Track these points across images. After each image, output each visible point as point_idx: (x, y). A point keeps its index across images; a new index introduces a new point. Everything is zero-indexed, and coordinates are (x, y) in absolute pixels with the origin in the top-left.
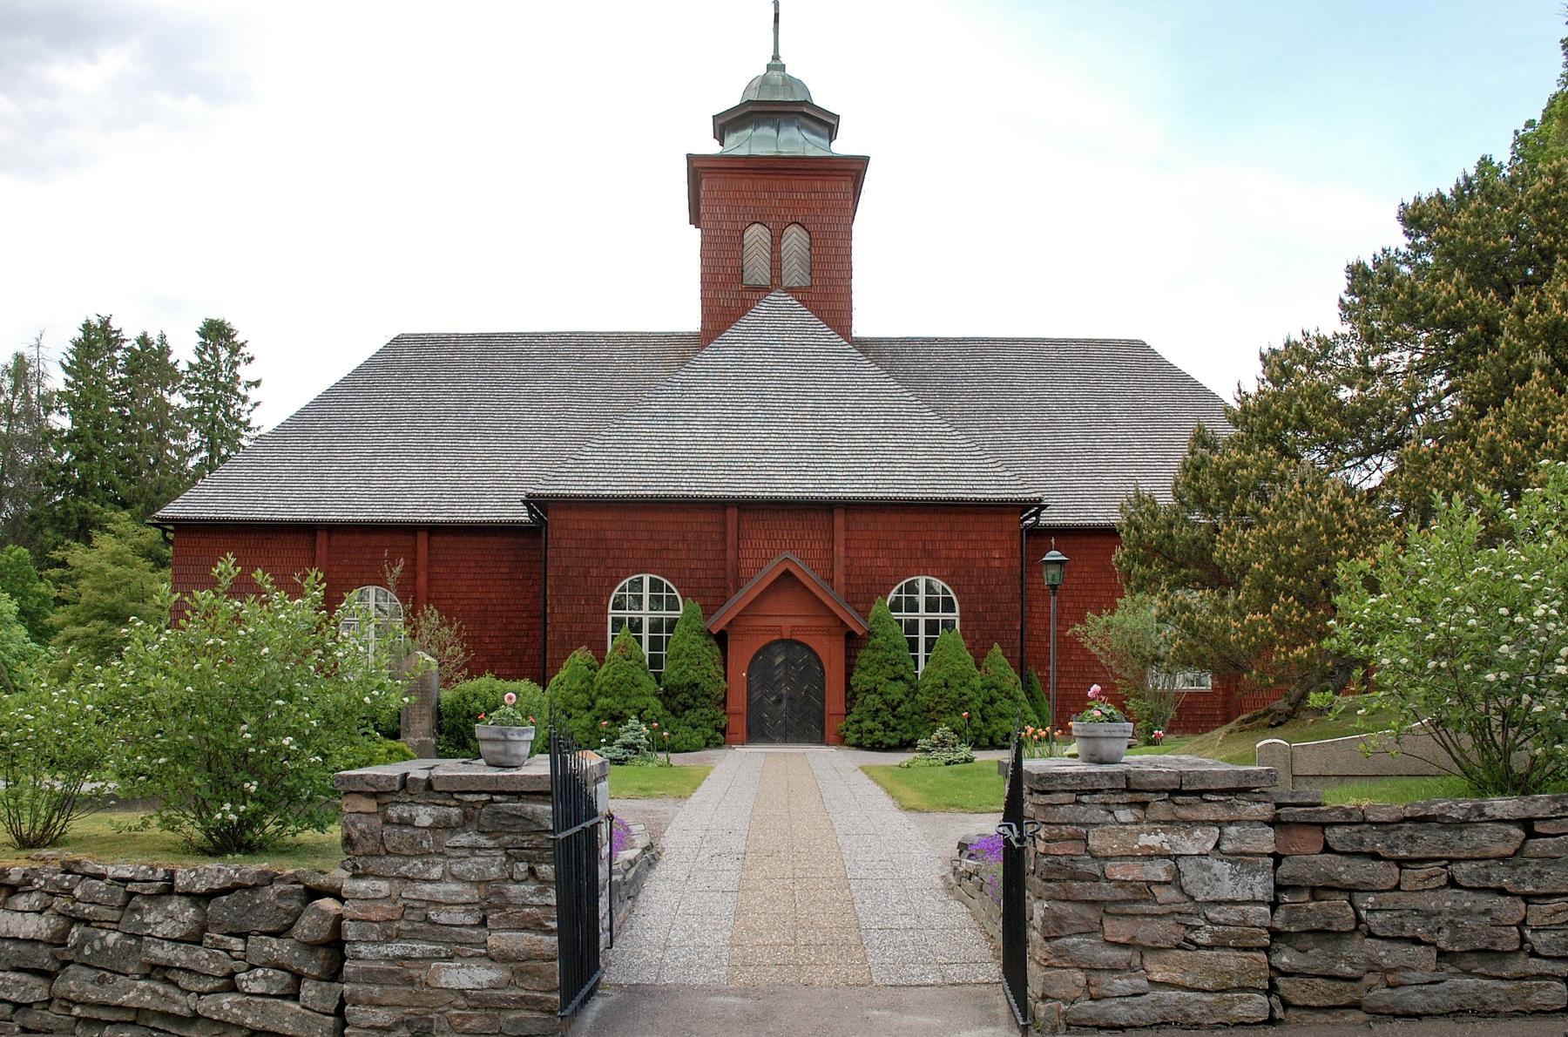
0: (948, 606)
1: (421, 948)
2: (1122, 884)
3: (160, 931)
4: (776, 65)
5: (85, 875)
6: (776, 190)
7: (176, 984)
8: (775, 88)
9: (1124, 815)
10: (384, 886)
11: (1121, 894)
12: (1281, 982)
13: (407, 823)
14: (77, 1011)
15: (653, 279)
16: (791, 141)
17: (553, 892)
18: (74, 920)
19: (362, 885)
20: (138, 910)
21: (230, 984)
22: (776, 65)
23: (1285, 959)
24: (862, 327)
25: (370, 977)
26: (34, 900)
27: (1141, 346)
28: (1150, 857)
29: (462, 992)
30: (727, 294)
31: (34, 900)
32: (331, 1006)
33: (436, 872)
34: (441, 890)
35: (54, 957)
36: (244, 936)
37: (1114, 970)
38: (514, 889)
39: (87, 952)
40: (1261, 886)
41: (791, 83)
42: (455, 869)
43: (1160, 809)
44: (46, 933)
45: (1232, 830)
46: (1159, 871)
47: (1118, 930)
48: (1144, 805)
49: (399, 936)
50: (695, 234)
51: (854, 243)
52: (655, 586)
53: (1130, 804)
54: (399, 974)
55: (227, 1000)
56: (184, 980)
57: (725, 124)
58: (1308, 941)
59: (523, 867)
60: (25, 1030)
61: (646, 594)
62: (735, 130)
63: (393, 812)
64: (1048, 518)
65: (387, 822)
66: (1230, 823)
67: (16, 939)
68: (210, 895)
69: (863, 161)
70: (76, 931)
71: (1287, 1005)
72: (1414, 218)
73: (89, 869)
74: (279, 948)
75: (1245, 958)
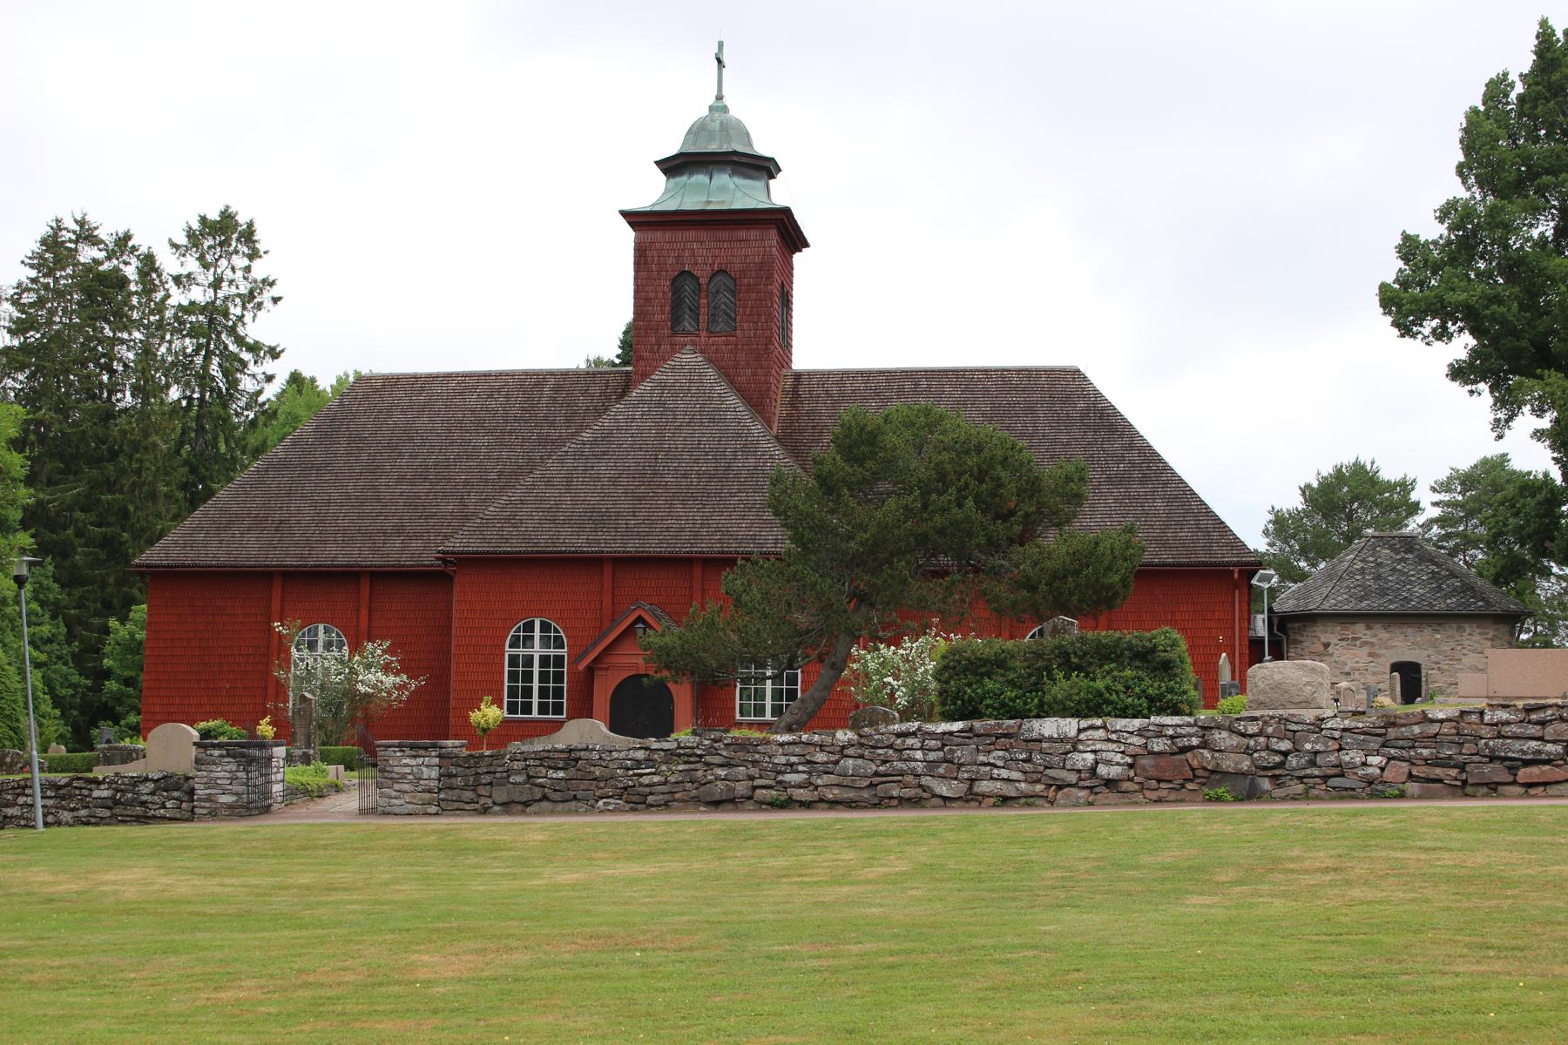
4: (719, 106)
16: (723, 189)
18: (117, 791)
22: (719, 106)
25: (200, 800)
27: (1076, 373)
34: (221, 774)
40: (434, 773)
43: (408, 752)
46: (408, 770)
47: (396, 786)
51: (795, 279)
52: (545, 627)
54: (209, 799)
57: (672, 166)
74: (176, 794)
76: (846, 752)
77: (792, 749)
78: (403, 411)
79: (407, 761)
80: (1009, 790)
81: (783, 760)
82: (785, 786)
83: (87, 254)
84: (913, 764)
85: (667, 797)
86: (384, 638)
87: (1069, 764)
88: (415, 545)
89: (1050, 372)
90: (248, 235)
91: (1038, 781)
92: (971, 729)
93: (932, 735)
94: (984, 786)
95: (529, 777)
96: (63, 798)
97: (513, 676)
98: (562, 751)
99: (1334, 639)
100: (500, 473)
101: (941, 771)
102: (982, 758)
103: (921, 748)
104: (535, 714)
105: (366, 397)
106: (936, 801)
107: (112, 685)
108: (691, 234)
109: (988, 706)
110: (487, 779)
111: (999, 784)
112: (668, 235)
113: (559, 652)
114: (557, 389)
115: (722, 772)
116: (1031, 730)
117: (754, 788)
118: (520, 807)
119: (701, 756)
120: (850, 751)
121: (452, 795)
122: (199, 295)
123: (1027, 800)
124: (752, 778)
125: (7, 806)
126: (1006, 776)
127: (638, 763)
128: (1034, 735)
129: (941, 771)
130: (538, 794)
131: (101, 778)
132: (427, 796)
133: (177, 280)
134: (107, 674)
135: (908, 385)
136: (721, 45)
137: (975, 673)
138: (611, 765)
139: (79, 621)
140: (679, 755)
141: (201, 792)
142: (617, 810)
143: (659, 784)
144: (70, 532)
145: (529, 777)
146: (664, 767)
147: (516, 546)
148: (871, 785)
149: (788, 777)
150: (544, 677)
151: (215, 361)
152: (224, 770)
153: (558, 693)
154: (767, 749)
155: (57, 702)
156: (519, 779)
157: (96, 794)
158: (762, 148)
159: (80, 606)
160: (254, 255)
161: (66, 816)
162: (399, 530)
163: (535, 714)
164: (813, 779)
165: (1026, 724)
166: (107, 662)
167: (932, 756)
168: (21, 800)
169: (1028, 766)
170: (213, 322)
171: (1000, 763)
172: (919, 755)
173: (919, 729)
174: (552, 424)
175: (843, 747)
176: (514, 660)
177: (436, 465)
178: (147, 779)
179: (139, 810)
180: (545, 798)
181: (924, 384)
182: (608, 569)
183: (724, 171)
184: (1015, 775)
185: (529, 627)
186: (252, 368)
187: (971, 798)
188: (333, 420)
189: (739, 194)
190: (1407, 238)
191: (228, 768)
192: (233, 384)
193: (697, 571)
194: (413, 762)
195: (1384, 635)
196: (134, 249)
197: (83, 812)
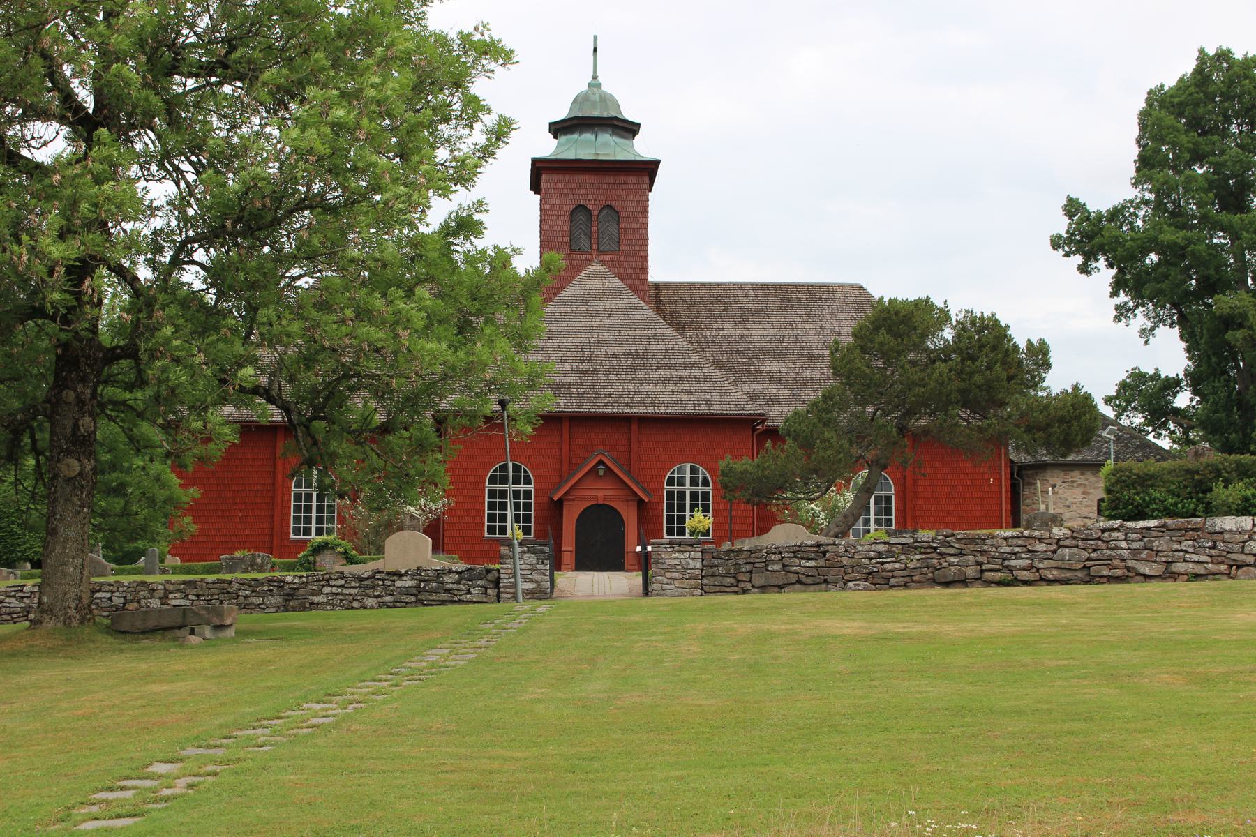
0: (705, 483)
4: (595, 84)
16: (606, 145)
21: (469, 592)
22: (595, 84)
23: (705, 581)
24: (657, 273)
25: (505, 587)
40: (699, 565)
41: (607, 100)
46: (677, 562)
47: (668, 575)
57: (558, 129)
62: (565, 134)
69: (657, 163)
74: (480, 583)
76: (1061, 543)
77: (1015, 541)
79: (676, 555)
80: (1200, 570)
81: (1008, 550)
82: (1010, 569)
84: (1120, 551)
85: (907, 579)
87: (1247, 550)
91: (1222, 563)
92: (1164, 525)
93: (1134, 530)
94: (1179, 567)
95: (784, 566)
96: (367, 587)
97: (492, 506)
98: (811, 546)
99: (1059, 482)
101: (1143, 555)
102: (1176, 546)
103: (1125, 540)
106: (1138, 578)
108: (585, 178)
109: (1153, 510)
110: (748, 568)
111: (1191, 565)
112: (567, 178)
113: (527, 487)
115: (955, 560)
116: (1213, 525)
117: (982, 571)
118: (776, 589)
119: (935, 548)
120: (1066, 543)
121: (712, 581)
123: (1214, 575)
124: (980, 564)
126: (1194, 558)
127: (880, 554)
128: (1217, 529)
129: (1143, 555)
130: (793, 578)
131: (403, 571)
132: (693, 582)
135: (741, 295)
136: (595, 38)
137: (1142, 485)
138: (857, 556)
140: (916, 548)
142: (866, 589)
143: (900, 569)
146: (903, 557)
148: (1085, 567)
149: (1013, 563)
154: (995, 542)
157: (399, 584)
158: (629, 114)
161: (370, 601)
164: (1036, 564)
165: (1209, 521)
167: (1135, 545)
168: (326, 590)
169: (1213, 552)
171: (1191, 550)
172: (1124, 544)
173: (1121, 526)
175: (1059, 540)
176: (492, 494)
179: (445, 596)
180: (799, 582)
183: (606, 131)
184: (1204, 558)
187: (1169, 575)
189: (618, 149)
190: (1070, 200)
193: (634, 427)
197: (387, 599)
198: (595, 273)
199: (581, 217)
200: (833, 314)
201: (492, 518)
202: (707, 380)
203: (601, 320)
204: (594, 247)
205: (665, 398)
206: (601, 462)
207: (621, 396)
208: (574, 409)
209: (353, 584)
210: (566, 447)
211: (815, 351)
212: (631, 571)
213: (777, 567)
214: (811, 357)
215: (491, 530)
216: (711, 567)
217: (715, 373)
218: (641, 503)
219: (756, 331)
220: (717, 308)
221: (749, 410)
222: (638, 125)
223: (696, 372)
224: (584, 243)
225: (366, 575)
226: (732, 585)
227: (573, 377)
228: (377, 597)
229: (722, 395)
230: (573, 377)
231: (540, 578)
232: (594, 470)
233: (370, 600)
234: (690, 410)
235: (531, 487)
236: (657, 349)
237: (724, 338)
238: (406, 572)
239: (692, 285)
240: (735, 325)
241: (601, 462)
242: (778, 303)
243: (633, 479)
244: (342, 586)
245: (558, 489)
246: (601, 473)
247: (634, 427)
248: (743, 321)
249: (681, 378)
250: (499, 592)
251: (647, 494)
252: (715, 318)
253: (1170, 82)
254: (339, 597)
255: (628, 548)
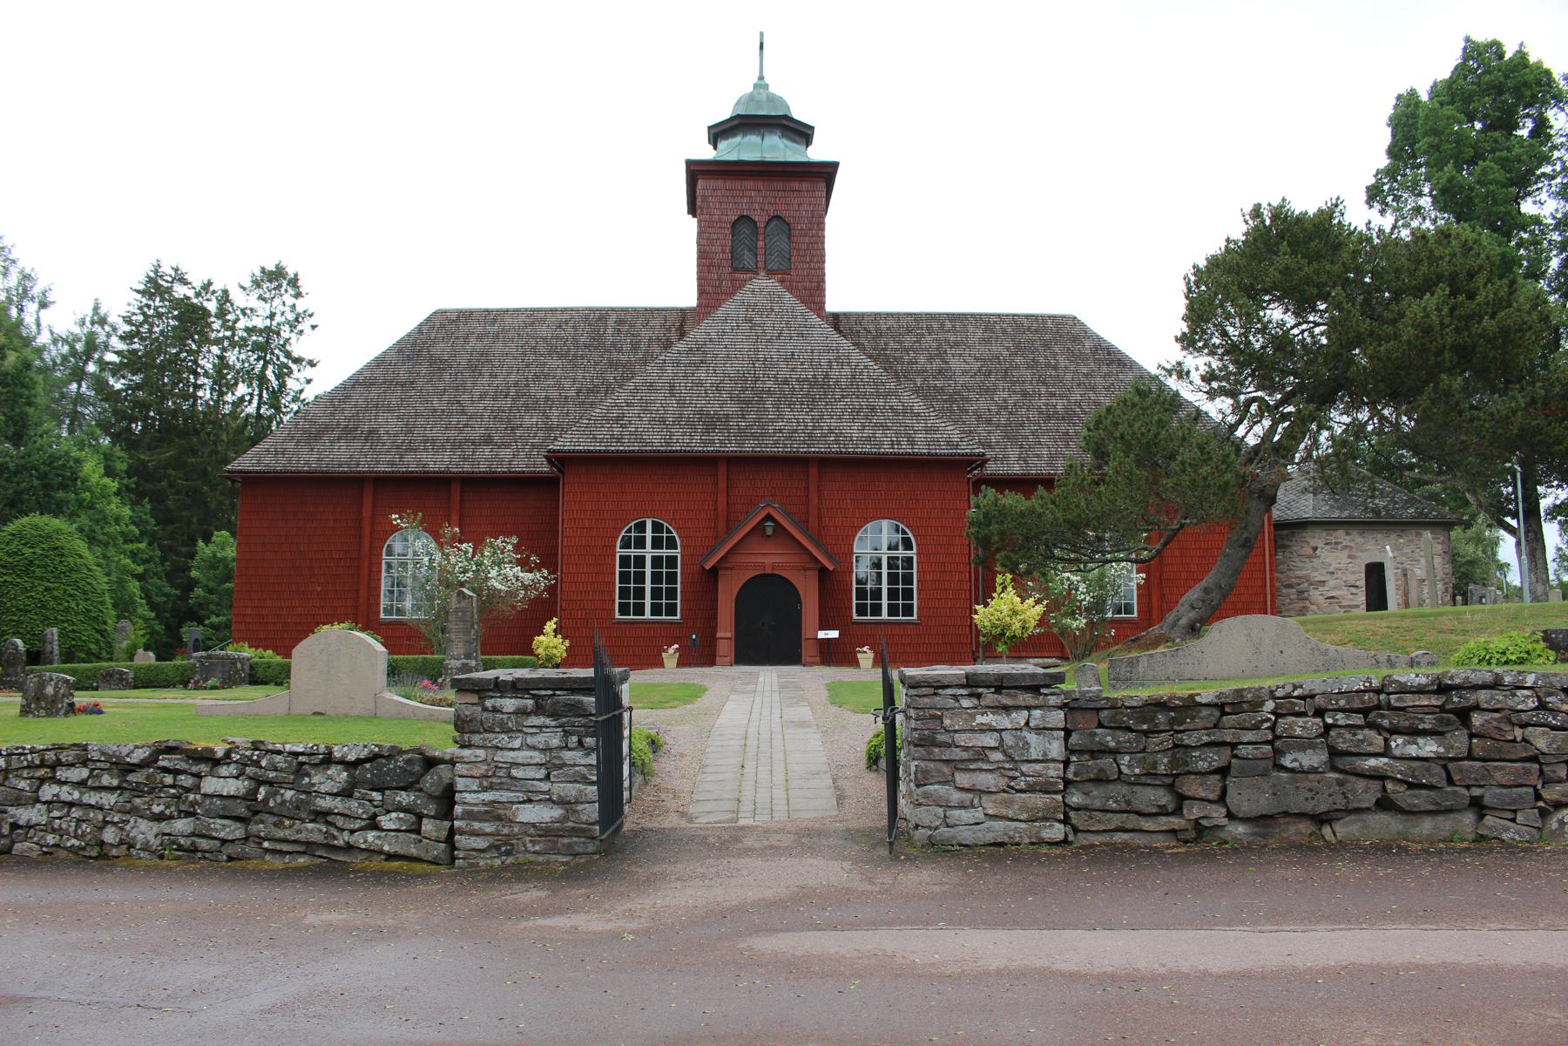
0: (671, 544)
1: (504, 796)
2: (966, 749)
3: (323, 789)
4: (761, 84)
5: (268, 751)
6: (760, 193)
7: (333, 825)
8: (759, 104)
9: (966, 703)
10: (481, 753)
11: (965, 755)
12: (1072, 814)
13: (495, 710)
14: (266, 844)
15: (653, 262)
17: (594, 756)
18: (259, 782)
19: (466, 752)
20: (308, 775)
21: (373, 824)
22: (761, 84)
23: (1075, 799)
25: (469, 815)
26: (233, 769)
28: (982, 731)
29: (533, 825)
30: (720, 269)
31: (233, 769)
32: (444, 834)
33: (517, 743)
35: (248, 807)
36: (381, 790)
37: (962, 807)
38: (568, 756)
39: (271, 804)
40: (1056, 749)
41: (773, 99)
42: (529, 740)
43: (990, 697)
44: (243, 791)
45: (1037, 713)
46: (990, 740)
47: (963, 779)
48: (979, 696)
49: (491, 787)
50: (692, 224)
51: (827, 233)
52: (657, 528)
53: (970, 695)
54: (493, 813)
55: (371, 836)
56: (340, 822)
57: (718, 133)
58: (1089, 787)
59: (575, 739)
60: (230, 859)
61: (649, 535)
62: (726, 138)
63: (489, 703)
64: (991, 468)
65: (485, 709)
66: (1036, 708)
67: (221, 796)
68: (358, 762)
69: (834, 166)
70: (262, 791)
71: (1076, 830)
72: (1521, 56)
73: (270, 747)
74: (404, 798)
75: (1046, 798)
78: (479, 338)
83: (180, 291)
86: (508, 535)
88: (506, 453)
89: (1053, 317)
90: (294, 282)
95: (1334, 752)
96: (137, 790)
97: (624, 577)
98: (1420, 691)
100: (579, 391)
104: (885, 616)
105: (443, 326)
107: (199, 591)
108: (750, 184)
112: (728, 184)
113: (671, 552)
114: (620, 322)
121: (1096, 797)
122: (260, 323)
125: (18, 802)
132: (1039, 800)
133: (243, 312)
134: (192, 584)
135: (935, 325)
136: (762, 34)
139: (171, 549)
141: (470, 796)
144: (164, 484)
145: (1334, 752)
147: (629, 446)
150: (656, 578)
151: (270, 368)
152: (528, 747)
153: (672, 594)
155: (153, 606)
156: (1310, 759)
157: (210, 785)
159: (172, 538)
160: (298, 295)
162: (488, 440)
163: (648, 615)
166: (194, 573)
168: (48, 792)
170: (265, 342)
174: (620, 351)
176: (625, 561)
177: (516, 384)
178: (328, 760)
179: (313, 831)
181: (948, 325)
182: (722, 468)
183: (771, 133)
185: (641, 527)
186: (296, 374)
188: (415, 344)
191: (539, 740)
192: (283, 385)
194: (1003, 721)
195: (1359, 540)
196: (214, 292)
197: (182, 825)
198: (762, 286)
199: (745, 230)
200: (1046, 346)
201: (624, 593)
202: (907, 411)
203: (769, 341)
204: (761, 264)
205: (853, 434)
206: (769, 517)
207: (796, 431)
208: (732, 448)
209: (106, 780)
210: (722, 500)
211: (1029, 388)
212: (811, 664)
213: (1312, 759)
214: (1025, 394)
215: (624, 609)
216: (1094, 754)
217: (918, 405)
218: (823, 571)
219: (956, 364)
220: (909, 340)
221: (965, 449)
222: (812, 128)
223: (894, 402)
224: (748, 259)
225: (135, 758)
226: (1163, 812)
227: (732, 408)
228: (159, 818)
229: (927, 430)
230: (732, 408)
231: (571, 790)
232: (759, 528)
233: (144, 825)
234: (886, 449)
235: (677, 552)
236: (841, 374)
237: (919, 372)
238: (228, 754)
239: (877, 316)
240: (930, 359)
241: (769, 517)
242: (979, 333)
243: (810, 539)
244: (82, 784)
245: (710, 555)
246: (769, 531)
247: (813, 471)
248: (941, 354)
249: (873, 409)
250: (452, 832)
251: (831, 560)
252: (906, 350)
253: (1445, 73)
254: (76, 813)
255: (806, 633)
